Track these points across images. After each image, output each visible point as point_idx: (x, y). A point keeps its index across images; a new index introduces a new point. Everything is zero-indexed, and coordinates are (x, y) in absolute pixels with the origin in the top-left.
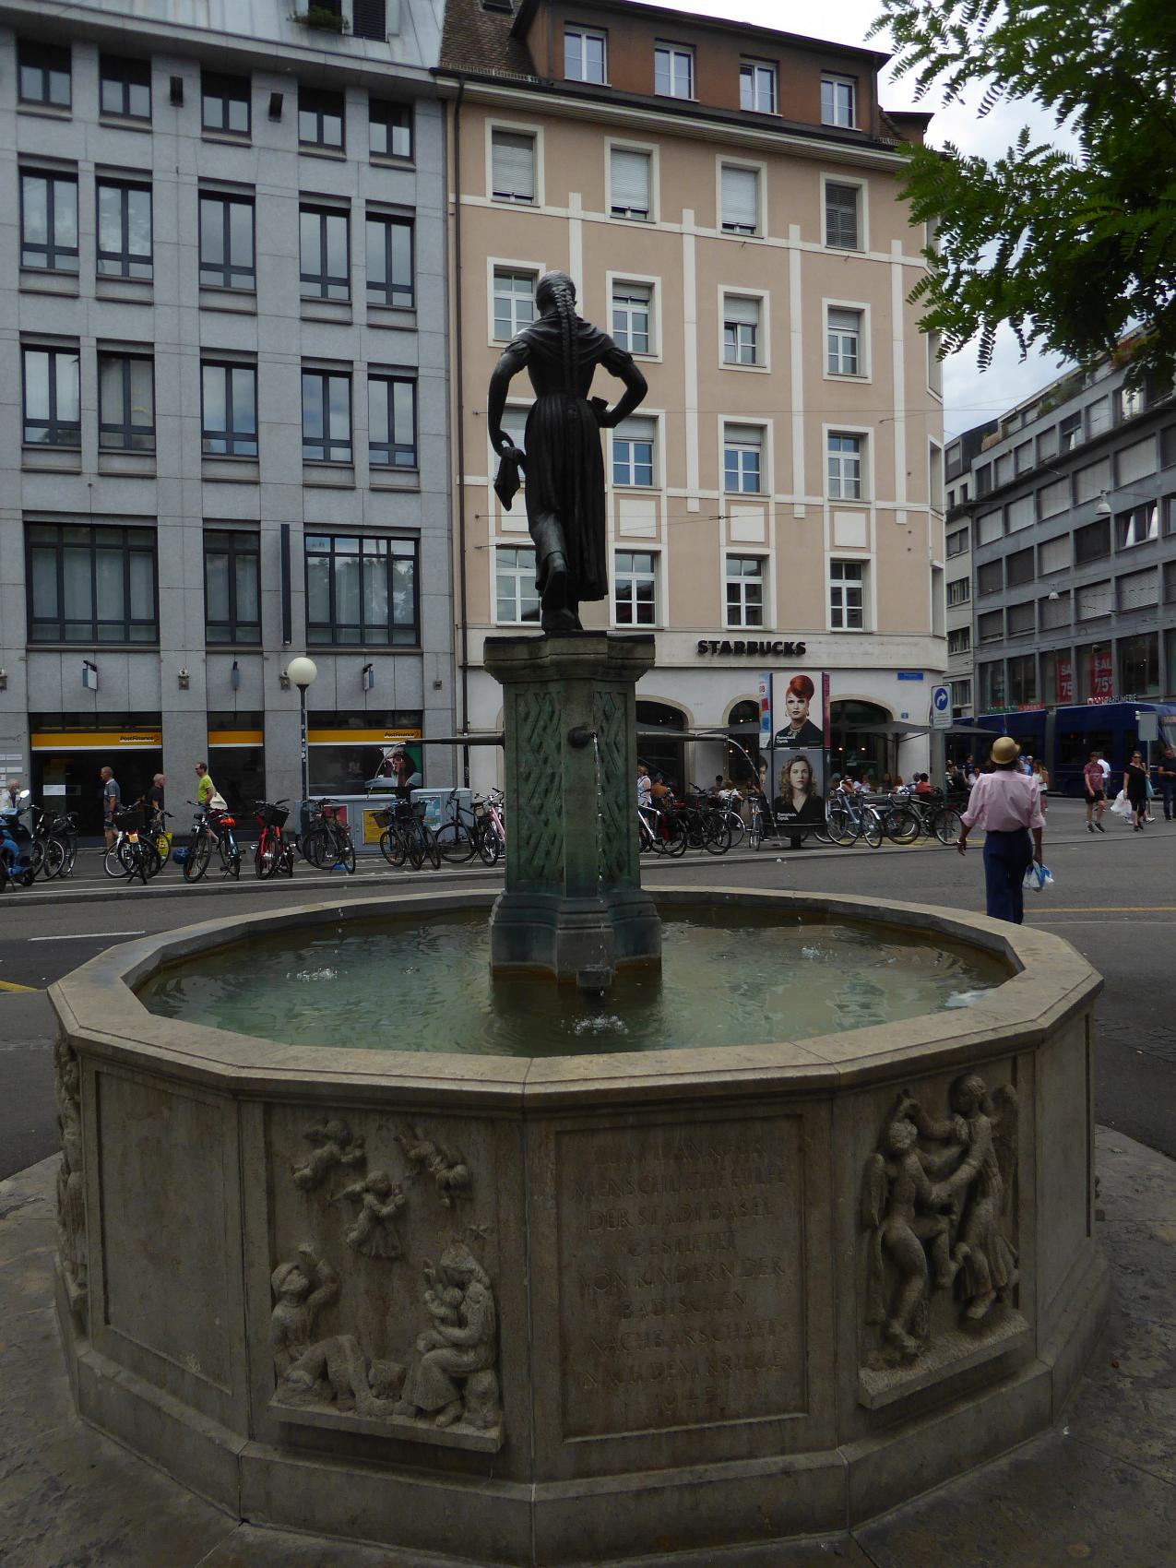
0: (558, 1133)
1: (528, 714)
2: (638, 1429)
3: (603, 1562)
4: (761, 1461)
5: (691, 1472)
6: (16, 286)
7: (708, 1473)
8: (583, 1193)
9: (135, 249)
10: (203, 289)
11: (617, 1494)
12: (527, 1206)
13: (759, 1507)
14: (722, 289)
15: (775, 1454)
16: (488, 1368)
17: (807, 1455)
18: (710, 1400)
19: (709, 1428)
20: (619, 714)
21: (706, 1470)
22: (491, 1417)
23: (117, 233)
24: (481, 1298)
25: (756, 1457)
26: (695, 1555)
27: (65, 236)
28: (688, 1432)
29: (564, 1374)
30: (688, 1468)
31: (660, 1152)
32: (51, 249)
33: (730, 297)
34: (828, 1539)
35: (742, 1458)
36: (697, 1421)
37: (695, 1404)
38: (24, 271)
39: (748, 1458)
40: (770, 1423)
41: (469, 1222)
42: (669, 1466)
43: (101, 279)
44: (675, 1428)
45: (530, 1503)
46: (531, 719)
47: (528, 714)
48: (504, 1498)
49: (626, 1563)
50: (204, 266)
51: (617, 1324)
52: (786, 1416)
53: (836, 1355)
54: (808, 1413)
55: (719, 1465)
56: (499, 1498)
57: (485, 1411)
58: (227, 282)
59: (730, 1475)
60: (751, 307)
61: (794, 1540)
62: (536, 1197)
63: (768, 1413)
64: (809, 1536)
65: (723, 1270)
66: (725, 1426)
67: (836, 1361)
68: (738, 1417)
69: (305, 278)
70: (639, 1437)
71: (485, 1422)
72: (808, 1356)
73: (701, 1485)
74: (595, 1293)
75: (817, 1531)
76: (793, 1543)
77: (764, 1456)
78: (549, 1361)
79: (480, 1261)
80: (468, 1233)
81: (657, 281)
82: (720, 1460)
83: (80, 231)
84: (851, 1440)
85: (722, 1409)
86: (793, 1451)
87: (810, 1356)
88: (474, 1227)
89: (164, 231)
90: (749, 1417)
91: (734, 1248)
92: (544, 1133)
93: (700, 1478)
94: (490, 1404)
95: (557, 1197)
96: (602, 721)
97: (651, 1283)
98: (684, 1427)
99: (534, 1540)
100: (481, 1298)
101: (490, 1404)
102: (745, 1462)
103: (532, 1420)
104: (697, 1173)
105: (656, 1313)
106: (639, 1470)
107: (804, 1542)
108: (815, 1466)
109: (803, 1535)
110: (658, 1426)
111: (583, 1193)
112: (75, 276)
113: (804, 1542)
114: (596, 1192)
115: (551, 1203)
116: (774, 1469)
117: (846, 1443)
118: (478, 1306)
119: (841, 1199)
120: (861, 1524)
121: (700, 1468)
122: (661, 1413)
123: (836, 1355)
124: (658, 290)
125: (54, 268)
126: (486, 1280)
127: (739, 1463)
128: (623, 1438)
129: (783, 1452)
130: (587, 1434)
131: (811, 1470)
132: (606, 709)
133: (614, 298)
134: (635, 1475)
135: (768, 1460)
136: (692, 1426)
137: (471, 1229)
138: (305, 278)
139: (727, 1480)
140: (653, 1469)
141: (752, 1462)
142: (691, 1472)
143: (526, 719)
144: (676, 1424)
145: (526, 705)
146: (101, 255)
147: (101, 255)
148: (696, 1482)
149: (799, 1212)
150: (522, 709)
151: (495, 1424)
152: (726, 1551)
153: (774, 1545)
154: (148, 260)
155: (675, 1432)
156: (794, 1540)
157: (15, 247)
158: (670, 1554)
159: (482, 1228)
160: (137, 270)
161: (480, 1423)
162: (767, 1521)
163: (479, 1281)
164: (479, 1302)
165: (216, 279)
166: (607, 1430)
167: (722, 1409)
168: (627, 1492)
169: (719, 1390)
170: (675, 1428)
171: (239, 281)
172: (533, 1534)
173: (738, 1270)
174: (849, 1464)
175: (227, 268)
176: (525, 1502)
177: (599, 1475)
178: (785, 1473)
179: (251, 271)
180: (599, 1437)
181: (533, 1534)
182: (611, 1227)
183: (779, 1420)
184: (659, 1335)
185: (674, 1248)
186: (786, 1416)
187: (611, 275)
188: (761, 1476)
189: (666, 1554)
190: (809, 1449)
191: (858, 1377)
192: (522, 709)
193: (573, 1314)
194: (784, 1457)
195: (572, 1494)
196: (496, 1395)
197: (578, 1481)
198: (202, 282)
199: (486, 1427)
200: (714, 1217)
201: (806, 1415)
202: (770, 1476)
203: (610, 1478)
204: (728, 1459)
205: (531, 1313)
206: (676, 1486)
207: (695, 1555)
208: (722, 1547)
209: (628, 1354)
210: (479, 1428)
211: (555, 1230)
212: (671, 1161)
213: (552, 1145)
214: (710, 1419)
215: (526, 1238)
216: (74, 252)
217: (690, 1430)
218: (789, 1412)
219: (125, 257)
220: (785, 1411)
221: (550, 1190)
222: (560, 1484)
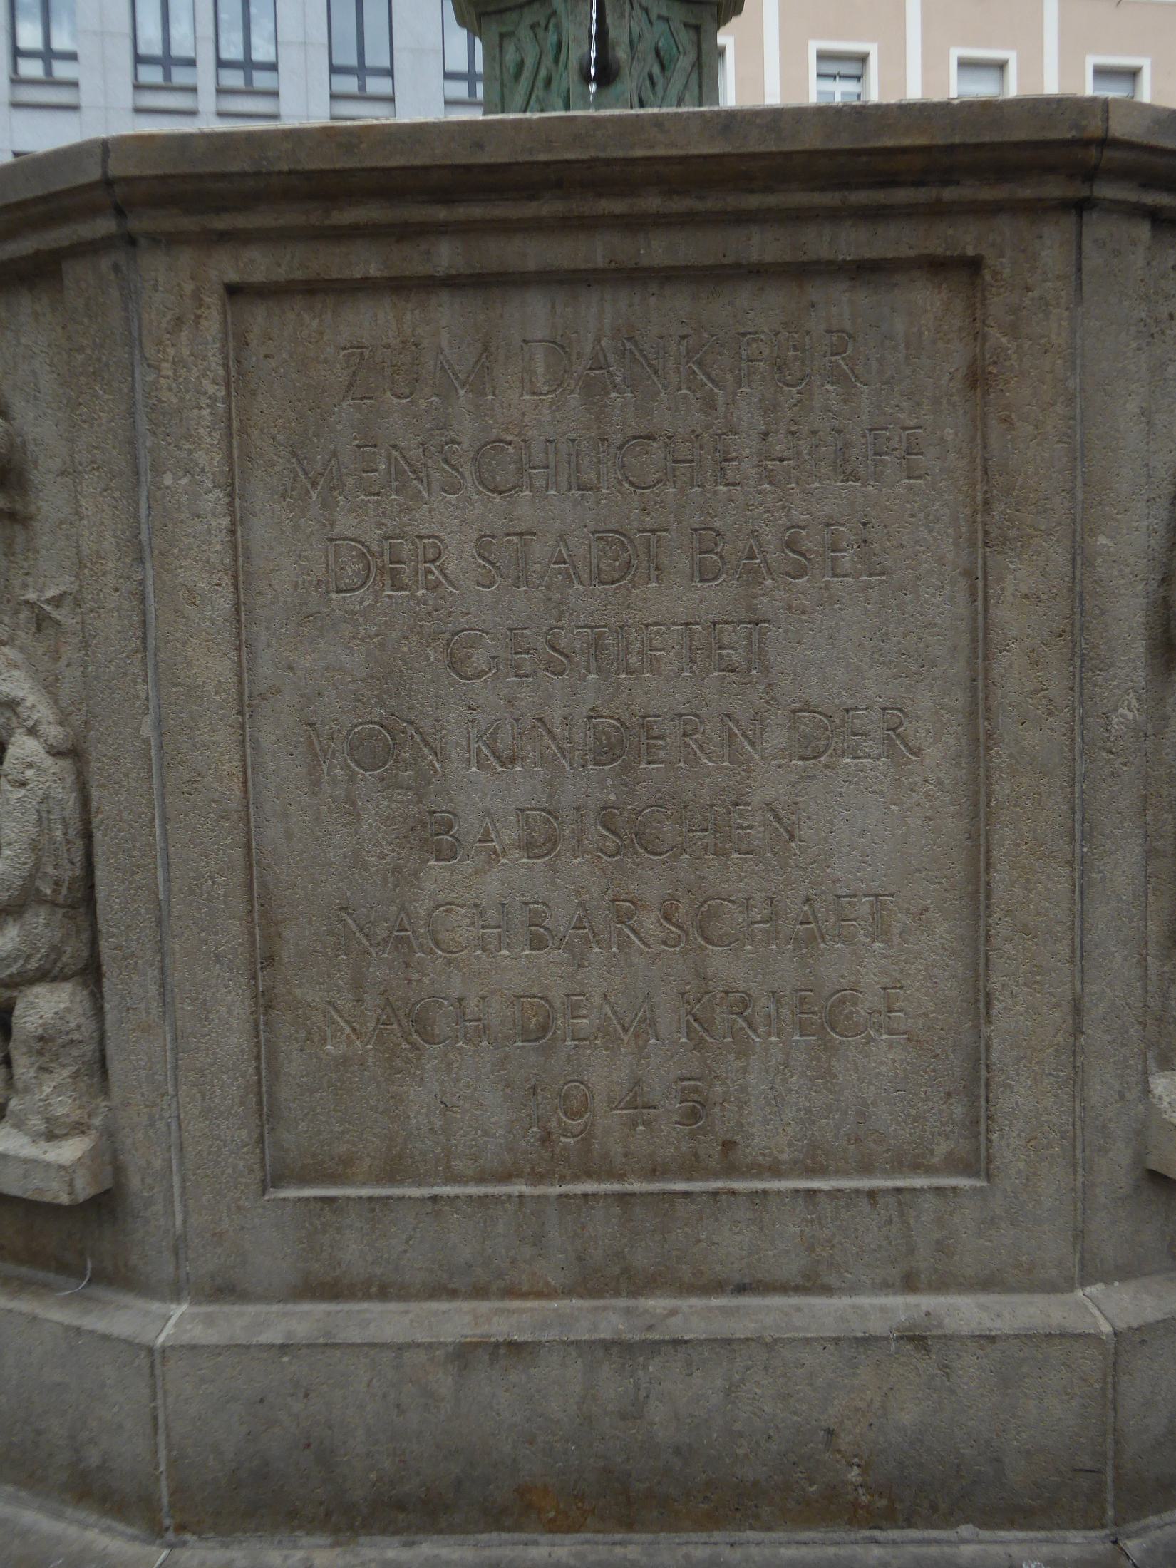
0: (233, 291)
1: (520, 66)
2: (481, 1179)
3: (362, 1539)
4: (840, 1303)
5: (628, 1311)
6: (129, 104)
7: (672, 1320)
8: (314, 484)
9: (257, 56)
10: (334, 97)
11: (400, 1348)
12: (143, 505)
13: (830, 1432)
14: (955, 53)
15: (885, 1287)
16: (66, 978)
17: (984, 1299)
18: (693, 1116)
19: (686, 1194)
20: (685, 62)
21: (673, 1312)
22: (63, 1107)
23: (238, 37)
24: (29, 773)
25: (827, 1290)
26: (633, 1552)
27: (181, 48)
28: (623, 1198)
29: (265, 1003)
30: (622, 1302)
31: (540, 369)
32: (167, 61)
33: (965, 64)
34: (1046, 1550)
35: (784, 1288)
36: (654, 1172)
37: (647, 1124)
38: (138, 87)
39: (798, 1290)
40: (872, 1194)
41: (25, 586)
42: (568, 1292)
43: (221, 91)
44: (589, 1187)
45: (150, 1351)
46: (527, 73)
47: (520, 66)
48: (92, 1332)
49: (429, 1548)
50: (334, 70)
51: (416, 874)
52: (919, 1182)
53: (1077, 1010)
54: (989, 1177)
55: (716, 1302)
56: (78, 1331)
57: (47, 1090)
58: (362, 87)
59: (741, 1328)
60: (994, 74)
61: (937, 1542)
62: (168, 480)
63: (866, 1169)
64: (985, 1534)
65: (731, 735)
66: (733, 1193)
67: (1078, 1031)
68: (776, 1171)
69: (448, 76)
70: (483, 1200)
71: (48, 1120)
72: (988, 1005)
73: (653, 1347)
74: (352, 778)
75: (1012, 1524)
76: (934, 1550)
77: (853, 1290)
78: (218, 960)
79: (50, 687)
80: (24, 614)
81: (872, 49)
82: (717, 1287)
83: (198, 35)
84: (1124, 1272)
85: (728, 1146)
86: (941, 1285)
87: (997, 1006)
88: (32, 596)
89: (289, 30)
90: (809, 1172)
91: (766, 670)
92: (189, 287)
93: (650, 1328)
94: (63, 1074)
95: (232, 487)
96: (652, 66)
97: (513, 761)
98: (617, 1187)
99: (162, 1453)
100: (29, 773)
101: (63, 1074)
102: (794, 1300)
103: (174, 1127)
104: (650, 437)
105: (529, 847)
106: (480, 1292)
107: (968, 1550)
108: (1007, 1330)
109: (966, 1530)
110: (538, 1177)
111: (314, 484)
112: (193, 90)
113: (968, 1550)
114: (350, 481)
115: (213, 499)
116: (877, 1326)
117: (1106, 1277)
118: (22, 792)
119: (1102, 540)
120: (1153, 1520)
121: (657, 1304)
122: (546, 1138)
123: (1077, 1010)
124: (873, 62)
125: (170, 80)
126: (54, 732)
127: (776, 1301)
128: (434, 1199)
129: (910, 1284)
130: (334, 1179)
131: (992, 1339)
132: (660, 44)
133: (820, 75)
134: (466, 1306)
135: (865, 1301)
136: (637, 1186)
137: (27, 602)
138: (448, 76)
139: (728, 1342)
140: (523, 1295)
141: (817, 1301)
142: (628, 1311)
143: (517, 76)
144: (590, 1175)
145: (517, 49)
146: (221, 64)
147: (221, 64)
148: (638, 1337)
149: (968, 573)
150: (511, 56)
151: (79, 1128)
152: (726, 1552)
153: (876, 1551)
154: (273, 67)
155: (585, 1195)
156: (937, 1542)
157: (127, 60)
158: (558, 1537)
159: (50, 593)
160: (262, 80)
161: (36, 1123)
162: (854, 1474)
163: (32, 731)
164: (23, 784)
165: (348, 84)
166: (391, 1174)
167: (728, 1146)
168: (430, 1346)
169: (719, 1089)
170: (589, 1187)
171: (376, 85)
172: (161, 1438)
173: (777, 737)
174: (1116, 1334)
175: (361, 70)
176: (140, 1346)
177: (367, 1297)
178: (911, 1339)
179: (389, 73)
180: (365, 1192)
181: (161, 1438)
182: (395, 587)
183: (899, 1190)
184: (537, 913)
185: (580, 658)
186: (919, 1182)
187: (814, 46)
188: (837, 1340)
189: (547, 1537)
190: (988, 1283)
191: (1147, 1091)
192: (511, 56)
193: (289, 835)
194: (912, 1299)
195: (273, 1336)
196: (89, 1049)
197: (306, 1307)
198: (333, 88)
199: (51, 1136)
200: (705, 574)
201: (985, 1184)
202: (866, 1341)
203: (392, 1306)
204: (741, 1289)
205: (165, 820)
206: (576, 1343)
207: (633, 1552)
208: (717, 1536)
209: (449, 962)
210: (36, 1137)
211: (227, 580)
212: (574, 399)
213: (212, 325)
214: (692, 1168)
215: (143, 600)
216: (191, 63)
217: (633, 1195)
218: (930, 1170)
219: (248, 65)
220: (918, 1167)
221: (209, 459)
222: (251, 1309)
